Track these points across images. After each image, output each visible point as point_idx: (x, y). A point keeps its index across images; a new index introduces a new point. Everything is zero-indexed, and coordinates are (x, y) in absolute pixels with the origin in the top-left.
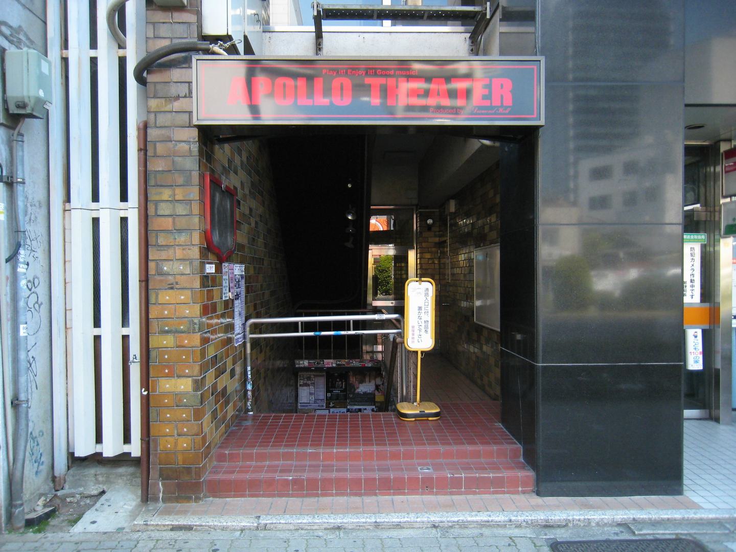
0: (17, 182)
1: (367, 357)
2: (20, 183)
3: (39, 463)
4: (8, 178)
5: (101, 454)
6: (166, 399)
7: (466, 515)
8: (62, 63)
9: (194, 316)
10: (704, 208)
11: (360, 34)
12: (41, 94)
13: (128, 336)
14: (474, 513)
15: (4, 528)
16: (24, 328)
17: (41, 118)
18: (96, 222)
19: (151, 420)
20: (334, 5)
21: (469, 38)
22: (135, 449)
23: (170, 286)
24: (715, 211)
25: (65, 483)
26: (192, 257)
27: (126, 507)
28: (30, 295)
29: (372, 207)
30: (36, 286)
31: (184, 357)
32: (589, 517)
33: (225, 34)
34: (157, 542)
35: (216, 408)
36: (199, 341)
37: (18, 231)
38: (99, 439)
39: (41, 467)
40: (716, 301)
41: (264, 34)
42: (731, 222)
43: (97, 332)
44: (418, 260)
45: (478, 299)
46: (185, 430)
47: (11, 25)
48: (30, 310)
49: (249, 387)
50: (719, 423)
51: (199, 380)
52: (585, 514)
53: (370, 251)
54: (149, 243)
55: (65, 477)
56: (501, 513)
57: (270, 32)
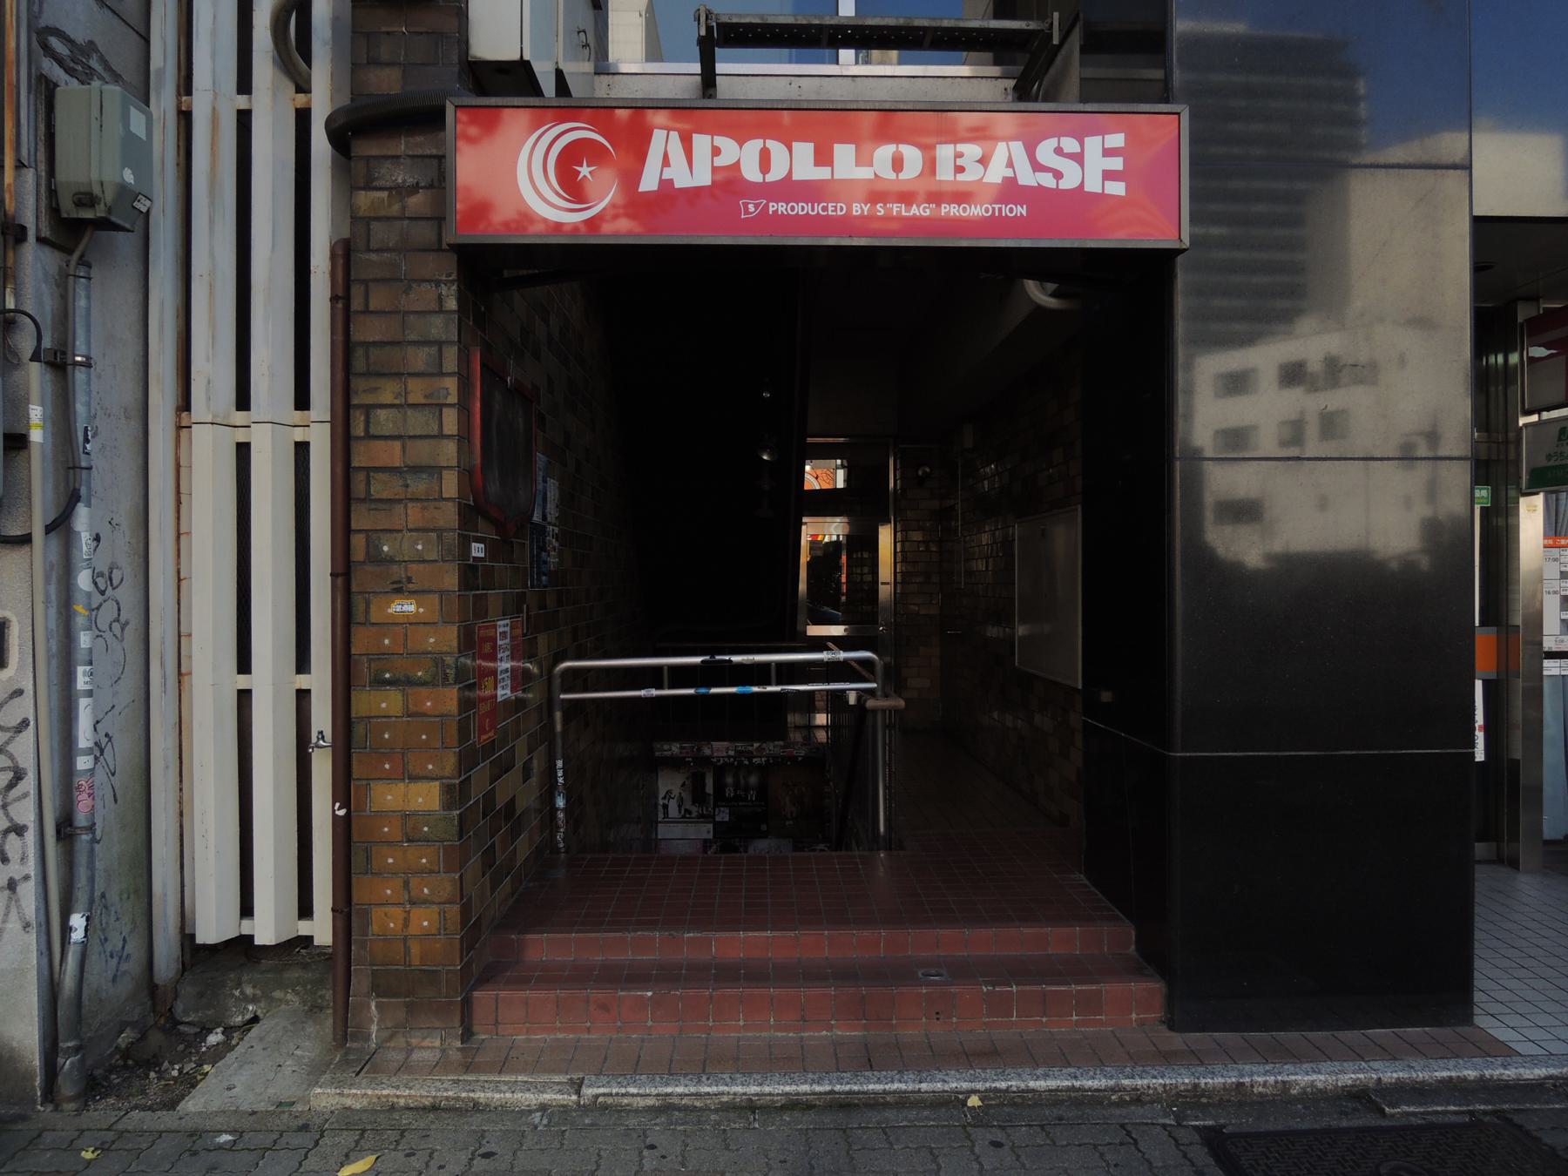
0: (76, 364)
1: (796, 736)
2: (80, 364)
3: (120, 958)
4: (55, 354)
5: (251, 937)
6: (385, 826)
7: (1025, 1076)
8: (179, 123)
9: (445, 649)
10: (1485, 434)
11: (792, 78)
12: (129, 176)
13: (308, 691)
14: (1040, 1071)
15: (39, 1099)
16: (84, 673)
17: (128, 231)
18: (243, 450)
19: (353, 871)
20: (740, 16)
21: (1014, 88)
22: (321, 929)
23: (395, 586)
24: (1507, 442)
25: (175, 999)
26: (441, 523)
27: (298, 1052)
28: (101, 605)
29: (809, 440)
30: (115, 582)
31: (424, 737)
32: (1286, 1078)
33: (516, 57)
34: (362, 1135)
35: (493, 844)
36: (455, 703)
37: (74, 468)
38: (247, 910)
39: (124, 967)
40: (1511, 623)
41: (597, 77)
42: (1542, 462)
43: (242, 682)
44: (899, 545)
45: (1023, 621)
46: (426, 891)
47: (72, 36)
48: (101, 636)
49: (560, 802)
50: (1518, 869)
51: (454, 785)
52: (1275, 1070)
53: (804, 527)
54: (353, 495)
55: (176, 987)
56: (1098, 1072)
57: (608, 74)
